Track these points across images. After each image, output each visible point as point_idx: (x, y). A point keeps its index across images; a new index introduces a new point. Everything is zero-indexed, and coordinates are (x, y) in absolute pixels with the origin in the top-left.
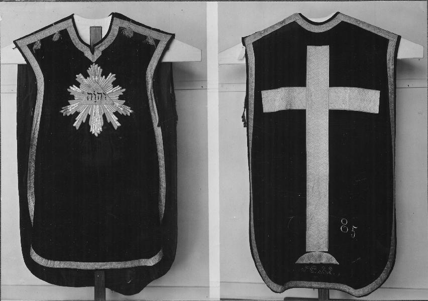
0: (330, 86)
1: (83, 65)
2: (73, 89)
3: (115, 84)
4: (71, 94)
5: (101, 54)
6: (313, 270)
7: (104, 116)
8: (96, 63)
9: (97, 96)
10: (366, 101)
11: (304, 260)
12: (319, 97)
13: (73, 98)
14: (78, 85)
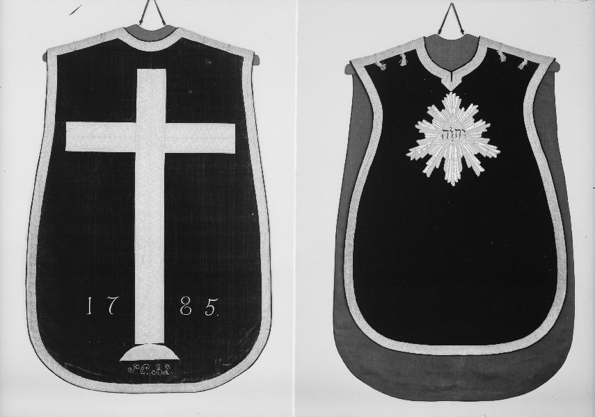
0: (168, 121)
1: (436, 93)
2: (422, 126)
3: (476, 118)
4: (420, 132)
5: (460, 82)
6: (145, 370)
7: (463, 160)
8: (453, 92)
9: (454, 133)
10: (215, 138)
11: (131, 355)
12: (150, 136)
13: (422, 136)
14: (430, 119)
